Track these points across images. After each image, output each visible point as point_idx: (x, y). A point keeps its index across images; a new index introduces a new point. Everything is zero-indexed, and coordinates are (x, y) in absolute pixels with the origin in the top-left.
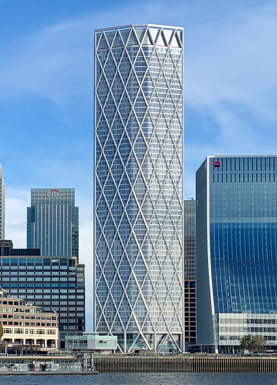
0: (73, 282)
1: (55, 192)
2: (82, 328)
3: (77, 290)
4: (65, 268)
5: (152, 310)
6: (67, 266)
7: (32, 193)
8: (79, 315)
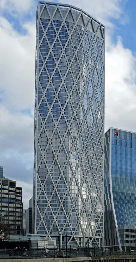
0: (13, 198)
2: (20, 233)
3: (16, 205)
4: (6, 187)
6: (8, 186)
8: (17, 223)
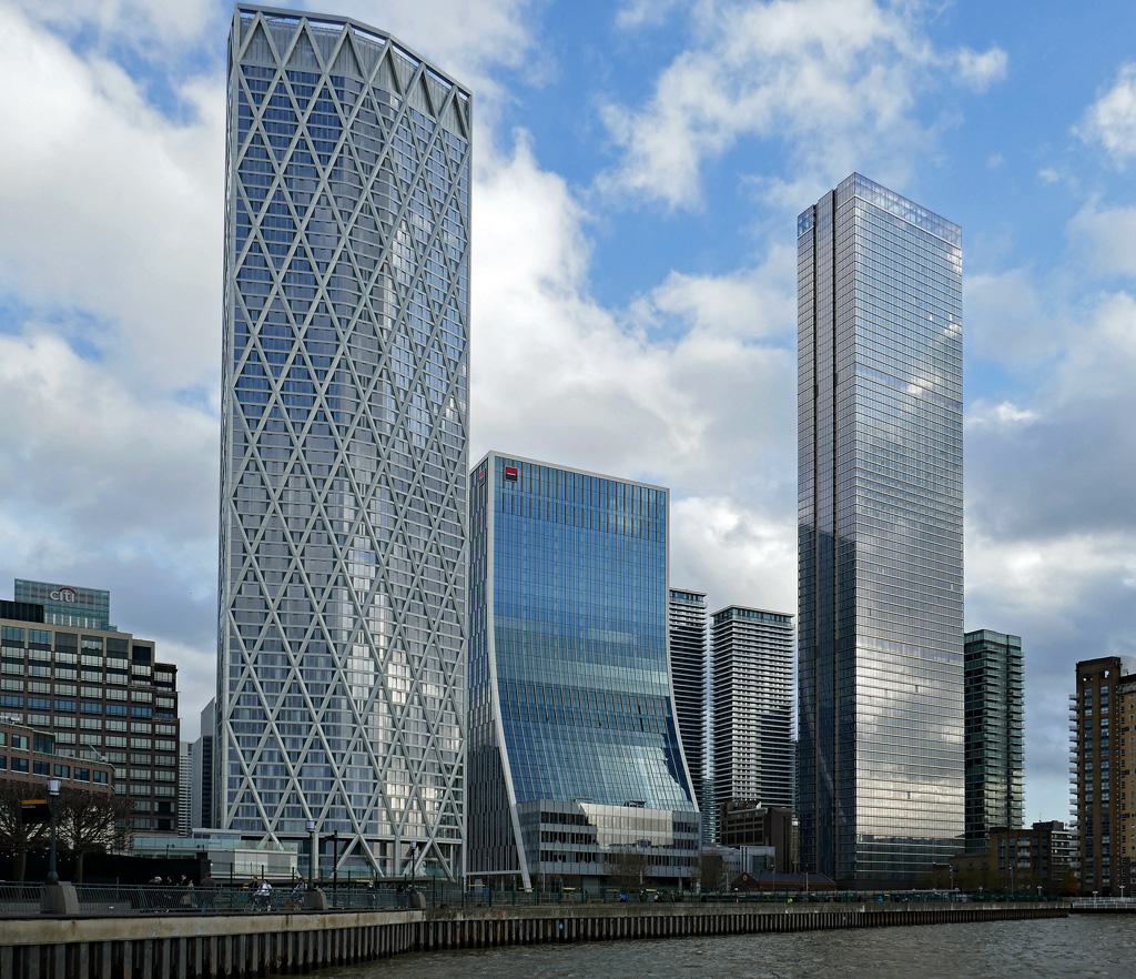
1: (67, 593)
3: (157, 726)
4: (122, 663)
5: (351, 777)
7: (16, 587)
